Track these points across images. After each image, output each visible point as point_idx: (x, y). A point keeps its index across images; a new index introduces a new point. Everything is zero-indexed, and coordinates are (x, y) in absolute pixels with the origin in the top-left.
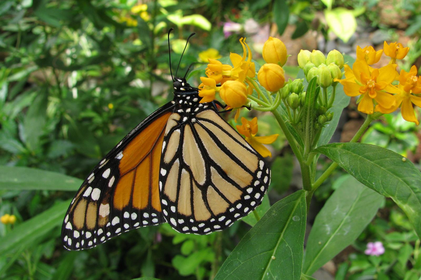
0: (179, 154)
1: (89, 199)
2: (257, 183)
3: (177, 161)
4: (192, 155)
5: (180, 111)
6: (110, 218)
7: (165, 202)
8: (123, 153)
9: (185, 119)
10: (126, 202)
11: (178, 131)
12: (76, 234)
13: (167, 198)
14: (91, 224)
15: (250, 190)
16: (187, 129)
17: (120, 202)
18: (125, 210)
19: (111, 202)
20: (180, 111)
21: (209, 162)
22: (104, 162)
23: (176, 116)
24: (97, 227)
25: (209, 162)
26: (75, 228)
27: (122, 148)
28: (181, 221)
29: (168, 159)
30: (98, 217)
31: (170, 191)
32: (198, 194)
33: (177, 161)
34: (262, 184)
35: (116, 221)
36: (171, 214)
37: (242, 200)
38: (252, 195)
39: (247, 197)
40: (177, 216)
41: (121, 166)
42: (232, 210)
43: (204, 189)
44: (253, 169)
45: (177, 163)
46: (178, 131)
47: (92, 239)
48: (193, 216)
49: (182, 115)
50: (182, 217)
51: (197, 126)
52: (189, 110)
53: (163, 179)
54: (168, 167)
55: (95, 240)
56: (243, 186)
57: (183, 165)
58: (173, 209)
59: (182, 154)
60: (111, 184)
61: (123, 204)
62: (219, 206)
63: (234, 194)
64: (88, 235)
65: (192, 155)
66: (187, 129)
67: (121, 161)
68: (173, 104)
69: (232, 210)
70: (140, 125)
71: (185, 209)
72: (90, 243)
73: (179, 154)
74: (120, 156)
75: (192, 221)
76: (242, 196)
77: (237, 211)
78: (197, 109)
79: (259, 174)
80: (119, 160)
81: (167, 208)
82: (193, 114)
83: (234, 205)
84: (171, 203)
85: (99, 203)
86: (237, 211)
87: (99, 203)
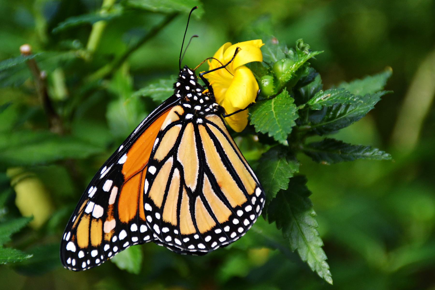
0: (173, 152)
1: (91, 217)
2: (248, 208)
3: (171, 159)
4: (188, 155)
5: (186, 105)
6: (116, 232)
7: (148, 207)
8: (127, 155)
9: (189, 116)
10: (133, 214)
11: (180, 126)
12: (81, 255)
13: (151, 203)
14: (97, 241)
15: (240, 213)
16: (190, 127)
17: (126, 216)
18: (131, 222)
19: (116, 216)
20: (186, 105)
21: (204, 168)
22: (105, 171)
23: (179, 109)
24: (104, 242)
25: (204, 168)
26: (78, 249)
27: (126, 151)
28: (166, 230)
29: (159, 156)
30: (103, 234)
31: (157, 196)
32: (186, 198)
33: (171, 159)
34: (253, 212)
35: (123, 235)
36: (155, 221)
37: (229, 222)
38: (241, 219)
39: (236, 222)
40: (162, 224)
41: (124, 172)
42: (218, 231)
43: (193, 196)
44: (250, 192)
45: (198, 199)
46: (180, 126)
47: (98, 257)
48: (178, 227)
49: (187, 111)
50: (168, 225)
51: (202, 129)
52: (198, 108)
53: (151, 178)
54: (159, 165)
55: (102, 257)
56: (234, 205)
57: (177, 165)
58: (158, 216)
59: (177, 152)
60: (112, 201)
61: (130, 216)
62: (206, 223)
63: (223, 214)
64: (94, 253)
65: (188, 155)
66: (190, 127)
67: (124, 166)
68: (177, 98)
69: (218, 231)
70: (143, 123)
71: (169, 216)
72: (98, 261)
73: (173, 152)
74: (122, 160)
75: (176, 232)
76: (231, 218)
77: (223, 234)
78: (207, 110)
79: (254, 200)
80: (122, 165)
81: (152, 214)
82: (202, 113)
83: (219, 225)
84: (155, 209)
85: (104, 219)
86: (223, 234)
87: (104, 219)
